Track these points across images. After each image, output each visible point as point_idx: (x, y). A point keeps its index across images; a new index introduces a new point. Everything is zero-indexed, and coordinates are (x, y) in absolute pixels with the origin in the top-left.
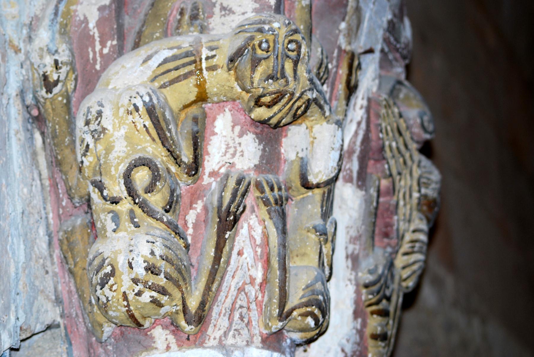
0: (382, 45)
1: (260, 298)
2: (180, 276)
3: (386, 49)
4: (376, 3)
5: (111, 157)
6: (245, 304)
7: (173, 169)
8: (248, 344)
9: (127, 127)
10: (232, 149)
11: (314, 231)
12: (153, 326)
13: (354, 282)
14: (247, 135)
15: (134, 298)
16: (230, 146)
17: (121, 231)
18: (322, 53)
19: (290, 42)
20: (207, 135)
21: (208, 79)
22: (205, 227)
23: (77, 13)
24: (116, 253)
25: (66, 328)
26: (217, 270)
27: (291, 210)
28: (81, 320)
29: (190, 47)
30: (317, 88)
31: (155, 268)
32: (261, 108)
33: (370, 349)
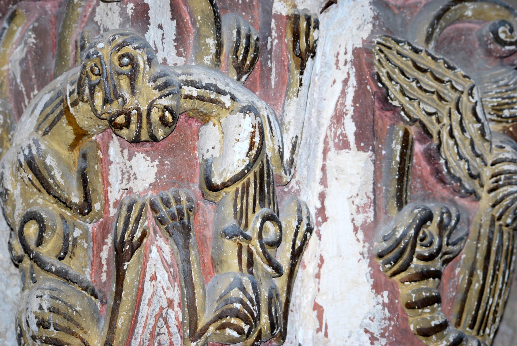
14: (135, 156)
31: (44, 322)
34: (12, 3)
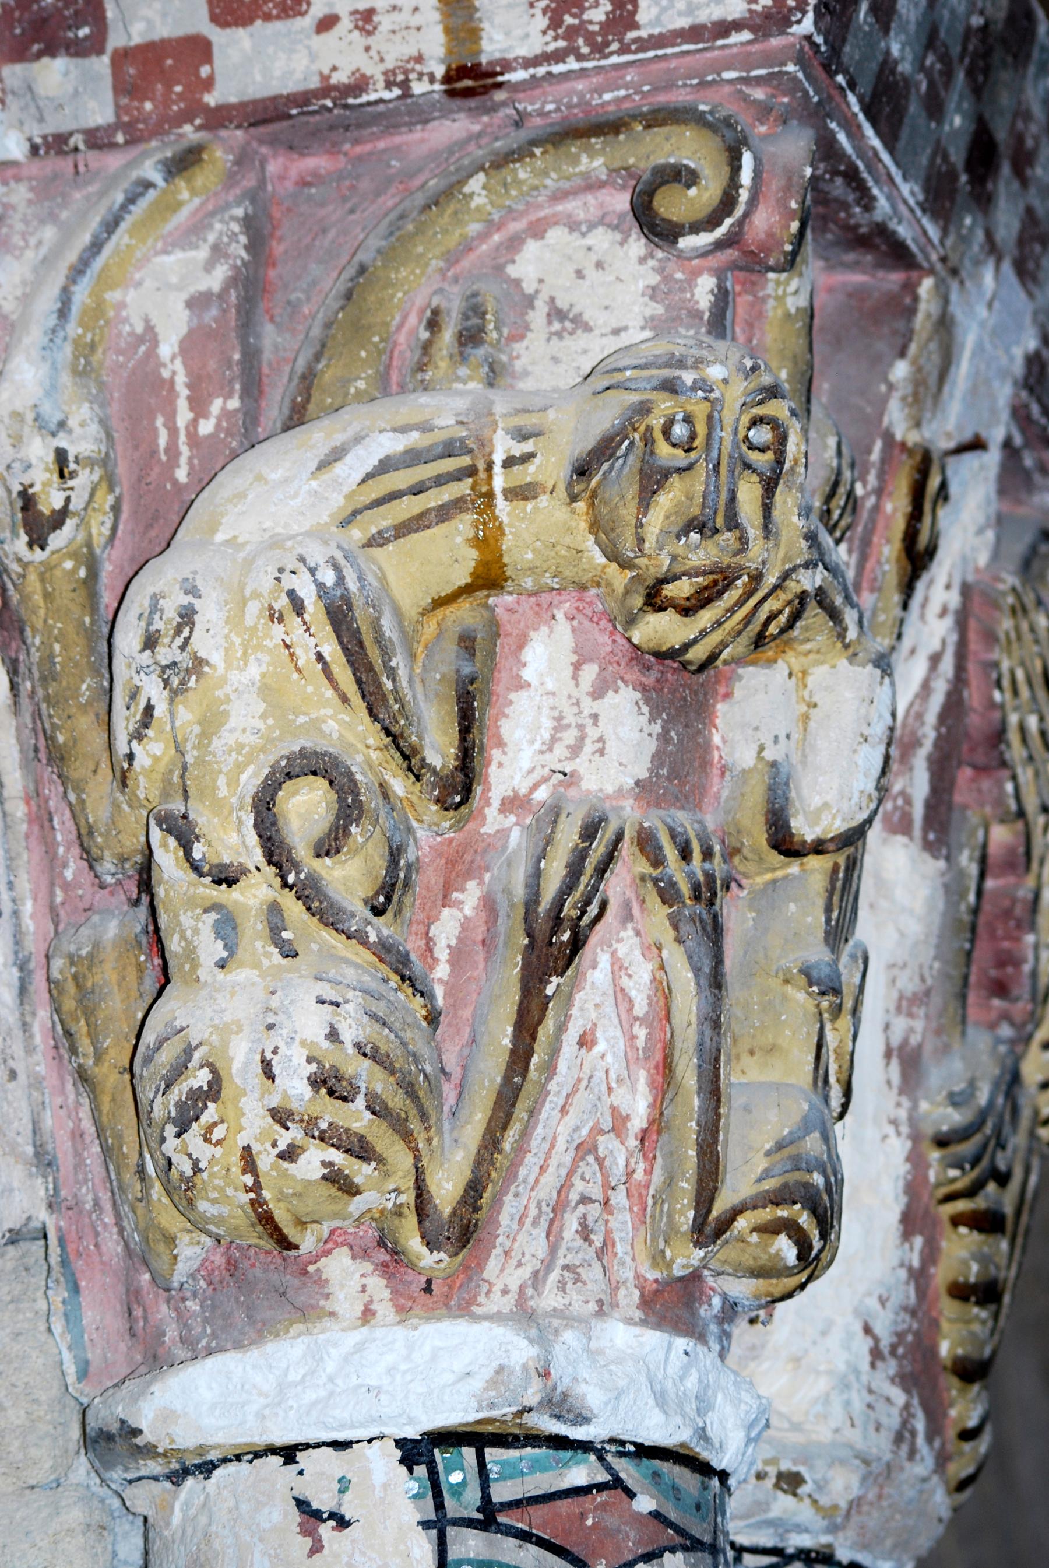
0: (1008, 425)
1: (639, 1175)
2: (412, 1105)
3: (1018, 440)
4: (997, 305)
5: (217, 744)
6: (595, 1192)
7: (400, 785)
8: (602, 1311)
9: (266, 658)
10: (568, 729)
11: (803, 980)
12: (329, 1244)
13: (905, 1129)
15: (274, 1167)
16: (565, 722)
17: (241, 965)
18: (839, 453)
19: (755, 422)
20: (499, 689)
21: (510, 525)
22: (487, 960)
23: (124, 314)
24: (226, 1031)
25: (62, 1242)
26: (519, 1089)
27: (737, 914)
28: (109, 1219)
29: (458, 427)
30: (827, 558)
31: (339, 1079)
32: (661, 614)
33: (945, 1325)
34: (198, 121)
